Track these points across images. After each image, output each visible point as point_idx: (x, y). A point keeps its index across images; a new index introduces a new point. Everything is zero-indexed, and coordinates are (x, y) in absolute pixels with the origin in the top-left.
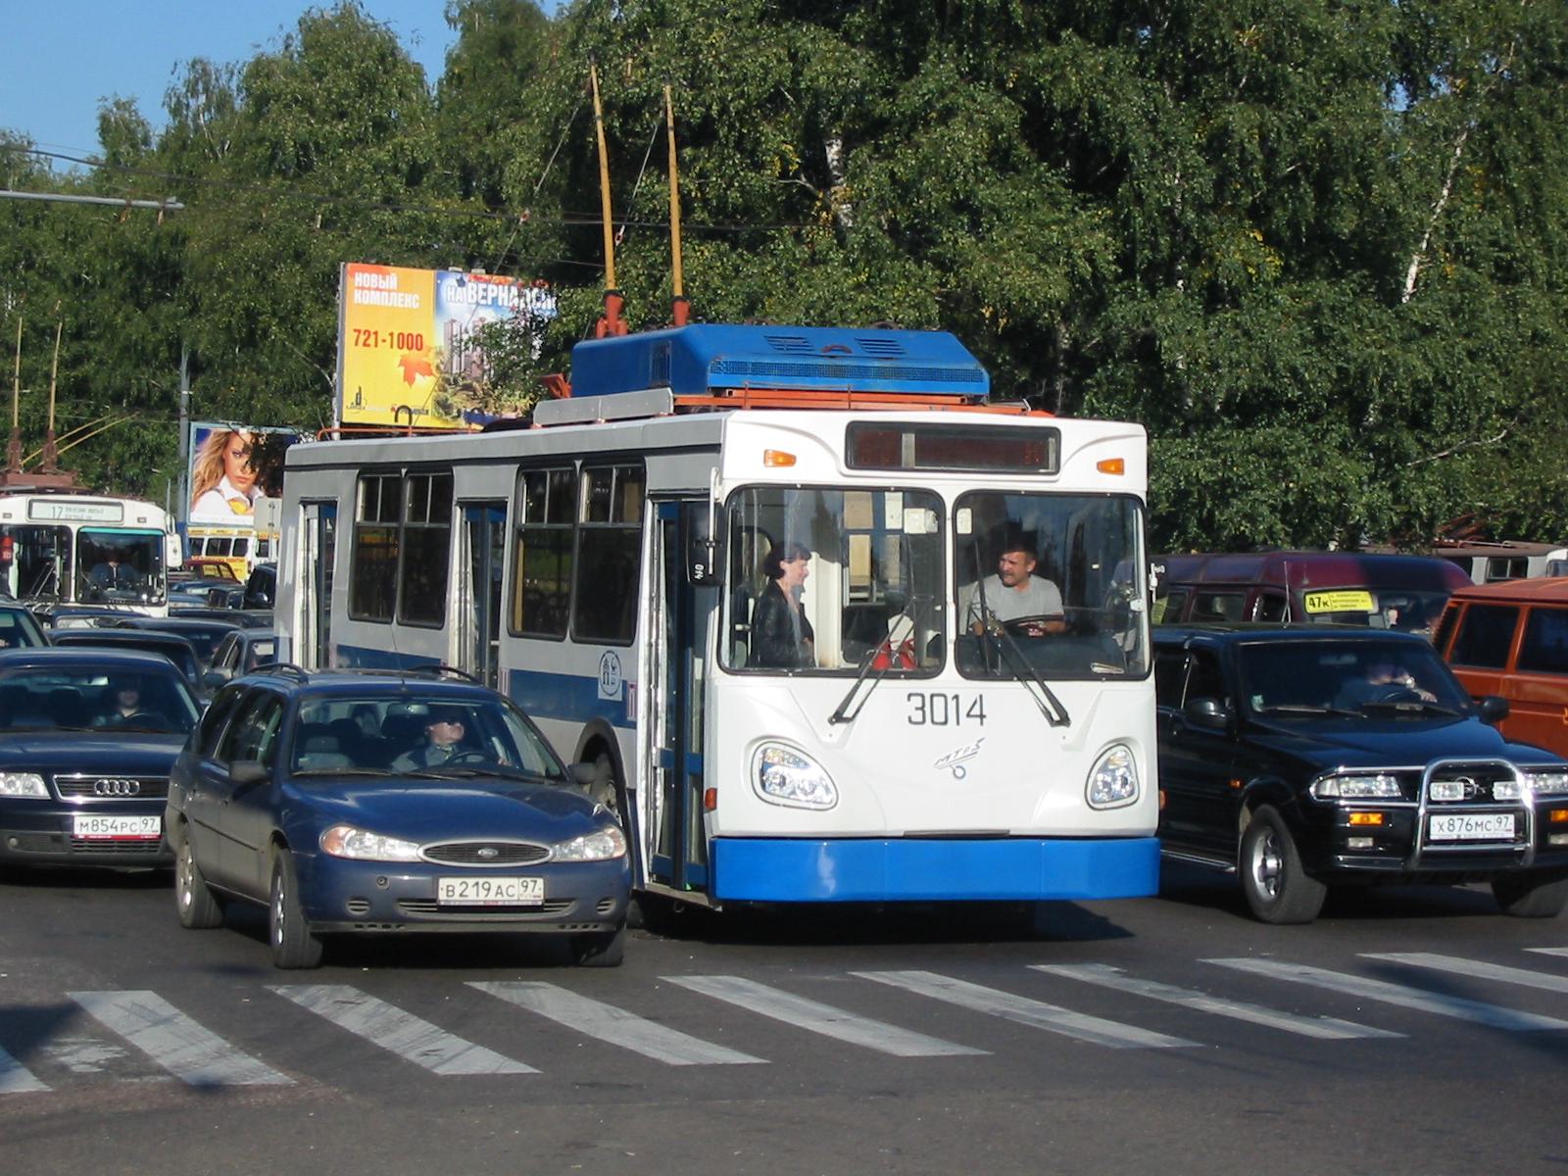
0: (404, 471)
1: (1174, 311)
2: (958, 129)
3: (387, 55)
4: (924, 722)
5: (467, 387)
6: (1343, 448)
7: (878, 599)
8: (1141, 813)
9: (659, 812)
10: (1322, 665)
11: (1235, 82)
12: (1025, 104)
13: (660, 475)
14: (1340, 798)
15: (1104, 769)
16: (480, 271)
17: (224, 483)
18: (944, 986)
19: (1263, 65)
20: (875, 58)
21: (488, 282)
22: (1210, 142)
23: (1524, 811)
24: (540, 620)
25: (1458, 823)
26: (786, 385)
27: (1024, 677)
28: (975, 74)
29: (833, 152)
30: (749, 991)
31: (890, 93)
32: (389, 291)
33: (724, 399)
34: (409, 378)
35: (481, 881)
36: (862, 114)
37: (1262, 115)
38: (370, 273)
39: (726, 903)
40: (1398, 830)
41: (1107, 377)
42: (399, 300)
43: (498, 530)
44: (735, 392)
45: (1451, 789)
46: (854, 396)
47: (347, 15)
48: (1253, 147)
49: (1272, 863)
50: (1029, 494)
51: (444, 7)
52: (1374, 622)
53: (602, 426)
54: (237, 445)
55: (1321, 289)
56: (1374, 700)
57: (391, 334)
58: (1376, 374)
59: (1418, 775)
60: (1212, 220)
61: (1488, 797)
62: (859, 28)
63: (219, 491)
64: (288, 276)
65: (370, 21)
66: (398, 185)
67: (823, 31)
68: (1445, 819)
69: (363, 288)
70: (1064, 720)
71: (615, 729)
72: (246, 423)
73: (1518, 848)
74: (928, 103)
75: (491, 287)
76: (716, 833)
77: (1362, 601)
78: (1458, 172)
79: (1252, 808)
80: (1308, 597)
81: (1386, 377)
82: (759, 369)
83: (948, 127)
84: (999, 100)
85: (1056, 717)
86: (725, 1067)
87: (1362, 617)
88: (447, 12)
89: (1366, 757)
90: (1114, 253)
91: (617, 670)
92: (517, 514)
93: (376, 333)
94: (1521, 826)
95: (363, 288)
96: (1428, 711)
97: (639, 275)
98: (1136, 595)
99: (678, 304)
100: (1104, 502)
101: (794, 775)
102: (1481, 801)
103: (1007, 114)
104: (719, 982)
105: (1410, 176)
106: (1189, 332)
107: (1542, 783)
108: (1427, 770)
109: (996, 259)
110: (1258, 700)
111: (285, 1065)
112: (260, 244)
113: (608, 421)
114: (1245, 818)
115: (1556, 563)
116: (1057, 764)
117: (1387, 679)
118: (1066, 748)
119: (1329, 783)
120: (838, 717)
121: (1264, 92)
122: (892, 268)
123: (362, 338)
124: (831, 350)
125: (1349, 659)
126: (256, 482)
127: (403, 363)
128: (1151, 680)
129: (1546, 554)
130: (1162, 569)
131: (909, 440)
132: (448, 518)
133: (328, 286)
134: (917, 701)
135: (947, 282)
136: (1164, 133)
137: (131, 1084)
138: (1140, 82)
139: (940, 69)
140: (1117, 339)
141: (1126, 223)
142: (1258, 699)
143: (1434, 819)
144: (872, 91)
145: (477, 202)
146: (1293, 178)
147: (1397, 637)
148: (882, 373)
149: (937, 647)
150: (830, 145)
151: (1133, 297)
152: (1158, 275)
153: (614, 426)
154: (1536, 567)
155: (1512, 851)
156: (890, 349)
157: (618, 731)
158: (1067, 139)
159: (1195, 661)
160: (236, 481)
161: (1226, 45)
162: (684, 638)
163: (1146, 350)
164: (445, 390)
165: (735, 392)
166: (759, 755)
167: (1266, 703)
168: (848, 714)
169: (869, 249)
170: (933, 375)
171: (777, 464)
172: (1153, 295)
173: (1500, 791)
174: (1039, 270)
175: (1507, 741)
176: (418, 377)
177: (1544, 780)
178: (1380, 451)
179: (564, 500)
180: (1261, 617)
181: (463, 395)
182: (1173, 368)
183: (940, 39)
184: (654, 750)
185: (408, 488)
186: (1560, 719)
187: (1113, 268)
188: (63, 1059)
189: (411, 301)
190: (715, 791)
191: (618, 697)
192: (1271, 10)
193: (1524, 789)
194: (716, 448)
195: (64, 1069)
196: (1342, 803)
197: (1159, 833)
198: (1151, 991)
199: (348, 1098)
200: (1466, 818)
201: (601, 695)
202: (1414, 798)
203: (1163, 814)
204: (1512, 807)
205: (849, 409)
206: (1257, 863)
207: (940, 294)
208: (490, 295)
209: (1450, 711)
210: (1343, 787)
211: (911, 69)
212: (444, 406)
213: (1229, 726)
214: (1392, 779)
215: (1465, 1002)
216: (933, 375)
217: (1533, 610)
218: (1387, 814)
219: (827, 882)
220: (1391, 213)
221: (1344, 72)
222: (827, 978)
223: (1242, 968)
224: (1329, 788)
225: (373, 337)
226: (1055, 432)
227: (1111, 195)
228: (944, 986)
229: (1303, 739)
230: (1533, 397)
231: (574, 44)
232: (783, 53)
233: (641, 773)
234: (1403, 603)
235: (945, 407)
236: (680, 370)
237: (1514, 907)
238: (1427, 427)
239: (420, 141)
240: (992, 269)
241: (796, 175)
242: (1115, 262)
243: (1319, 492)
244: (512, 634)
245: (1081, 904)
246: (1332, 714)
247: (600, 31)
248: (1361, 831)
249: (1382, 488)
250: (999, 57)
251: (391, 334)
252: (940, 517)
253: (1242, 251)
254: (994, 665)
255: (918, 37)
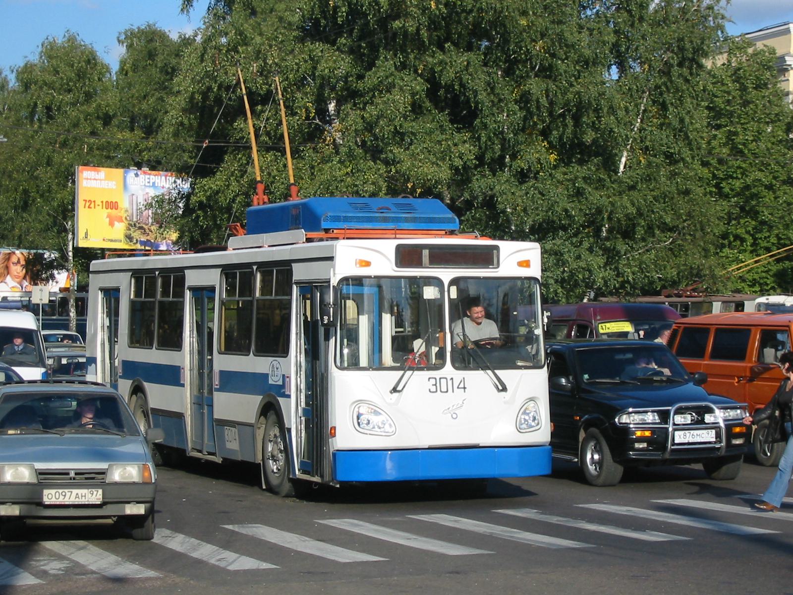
0: (157, 273)
1: (504, 183)
2: (397, 96)
3: (91, 60)
4: (436, 391)
5: (141, 228)
6: (590, 250)
7: (409, 332)
8: (543, 434)
9: (303, 439)
10: (611, 358)
11: (533, 68)
12: (427, 81)
13: (300, 273)
14: (630, 424)
15: (525, 413)
16: (146, 169)
17: (9, 279)
18: (456, 521)
19: (547, 60)
20: (353, 60)
21: (150, 174)
22: (521, 98)
23: (719, 427)
24: (233, 346)
25: (688, 435)
26: (362, 227)
27: (485, 368)
28: (403, 66)
29: (332, 107)
30: (362, 526)
31: (360, 77)
32: (101, 180)
33: (330, 235)
34: (111, 224)
35: (60, 491)
36: (347, 88)
37: (548, 85)
38: (91, 171)
39: (341, 483)
40: (659, 439)
41: (472, 216)
42: (106, 185)
43: (212, 299)
44: (335, 231)
45: (684, 418)
46: (397, 232)
47: (72, 39)
48: (544, 101)
49: (596, 457)
50: (485, 278)
51: (117, 35)
52: (630, 337)
53: (266, 249)
54: (14, 259)
55: (578, 171)
56: (640, 375)
57: (102, 202)
58: (607, 211)
59: (668, 412)
60: (521, 138)
61: (702, 421)
62: (344, 45)
63: (5, 283)
64: (45, 174)
65: (83, 43)
66: (99, 124)
67: (327, 46)
68: (681, 433)
69: (87, 179)
70: (504, 389)
71: (279, 398)
72: (19, 247)
73: (717, 446)
74: (381, 82)
75: (152, 177)
76: (336, 448)
77: (626, 327)
78: (645, 111)
79: (585, 431)
80: (600, 325)
81: (611, 213)
82: (346, 219)
83: (391, 94)
84: (416, 79)
85: (500, 388)
86: (367, 563)
87: (625, 334)
88: (118, 38)
89: (643, 404)
90: (474, 154)
91: (279, 369)
92: (220, 294)
93: (94, 202)
94: (718, 435)
95: (87, 179)
96: (670, 382)
97: (235, 170)
98: (537, 327)
99: (293, 187)
100: (519, 283)
101: (375, 419)
102: (699, 423)
103: (420, 86)
104: (345, 522)
105: (621, 113)
106: (513, 193)
107: (727, 414)
108: (672, 409)
109: (415, 160)
110: (586, 376)
111: (152, 567)
112: (29, 156)
113: (269, 246)
114: (582, 435)
115: (759, 305)
116: (501, 411)
117: (644, 365)
118: (505, 403)
119: (625, 416)
120: (395, 390)
121: (547, 72)
122: (362, 165)
123: (88, 204)
124: (381, 209)
125: (629, 356)
126: (24, 278)
127: (109, 216)
128: (546, 368)
129: (754, 299)
130: (549, 314)
131: (426, 253)
132: (182, 295)
133: (68, 177)
134: (433, 381)
135: (391, 171)
136: (498, 94)
137: (82, 579)
138: (485, 69)
139: (386, 64)
140: (476, 198)
141: (479, 139)
142: (586, 376)
143: (677, 433)
144: (352, 76)
145: (138, 133)
146: (563, 115)
147: (642, 344)
148: (406, 220)
149: (441, 355)
150: (330, 103)
151: (484, 176)
152: (498, 164)
153: (274, 248)
154: (750, 307)
155: (714, 447)
156: (410, 208)
157: (281, 400)
158: (446, 97)
159: (553, 358)
160: (14, 277)
161: (528, 50)
162: (314, 353)
163: (490, 203)
164: (130, 230)
165: (335, 231)
166: (356, 409)
167: (591, 377)
168: (399, 388)
169: (351, 155)
170: (431, 220)
171: (362, 266)
172: (494, 175)
173: (708, 418)
174: (437, 164)
175: (709, 395)
176: (116, 223)
177: (728, 412)
178: (606, 250)
179: (247, 287)
180: (576, 336)
181: (139, 232)
182: (504, 212)
183: (385, 48)
184: (299, 408)
185: (160, 281)
186: (733, 383)
187: (474, 161)
188: (42, 567)
189: (112, 185)
190: (335, 428)
191: (280, 383)
192: (550, 32)
193: (718, 416)
194: (331, 259)
195: (45, 573)
196: (631, 426)
197: (551, 444)
198: (557, 521)
199: (192, 582)
200: (692, 432)
201: (271, 382)
202: (666, 423)
203: (553, 435)
204: (715, 426)
205: (395, 238)
206: (589, 456)
207: (388, 177)
208: (152, 181)
209: (680, 380)
210: (632, 418)
211: (371, 65)
212: (129, 238)
213: (572, 390)
214: (655, 414)
215: (709, 522)
216: (431, 220)
217: (717, 330)
218: (653, 431)
219: (390, 472)
220: (611, 131)
221: (586, 63)
222: (396, 519)
223: (597, 508)
224: (625, 419)
225: (93, 204)
226: (497, 248)
227: (471, 124)
228: (456, 521)
229: (608, 394)
230: (685, 221)
231: (203, 55)
232: (307, 57)
233: (293, 420)
234: (647, 327)
235: (441, 236)
236: (306, 220)
237: (714, 475)
238: (632, 238)
239: (110, 100)
240: (414, 166)
241: (314, 118)
242: (475, 159)
243: (579, 272)
244: (220, 353)
245: (504, 480)
246: (623, 383)
247: (215, 48)
248: (641, 440)
249: (610, 269)
250: (415, 58)
251: (102, 202)
252: (442, 292)
253: (537, 153)
254: (469, 363)
255: (374, 49)
